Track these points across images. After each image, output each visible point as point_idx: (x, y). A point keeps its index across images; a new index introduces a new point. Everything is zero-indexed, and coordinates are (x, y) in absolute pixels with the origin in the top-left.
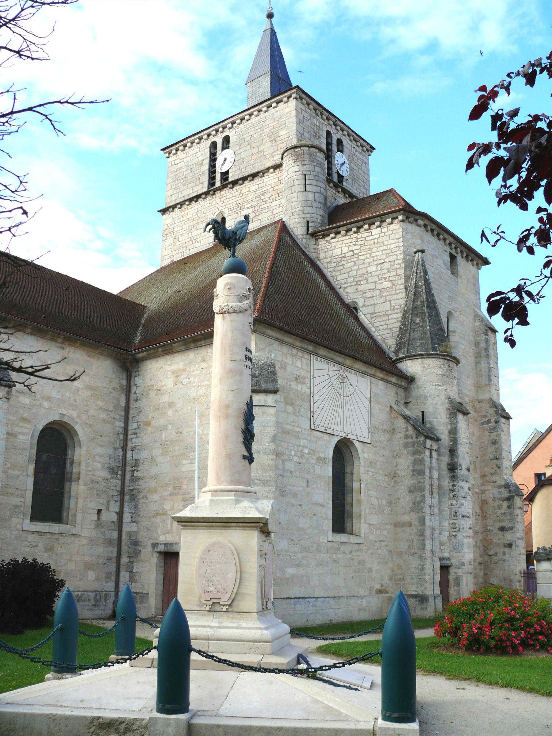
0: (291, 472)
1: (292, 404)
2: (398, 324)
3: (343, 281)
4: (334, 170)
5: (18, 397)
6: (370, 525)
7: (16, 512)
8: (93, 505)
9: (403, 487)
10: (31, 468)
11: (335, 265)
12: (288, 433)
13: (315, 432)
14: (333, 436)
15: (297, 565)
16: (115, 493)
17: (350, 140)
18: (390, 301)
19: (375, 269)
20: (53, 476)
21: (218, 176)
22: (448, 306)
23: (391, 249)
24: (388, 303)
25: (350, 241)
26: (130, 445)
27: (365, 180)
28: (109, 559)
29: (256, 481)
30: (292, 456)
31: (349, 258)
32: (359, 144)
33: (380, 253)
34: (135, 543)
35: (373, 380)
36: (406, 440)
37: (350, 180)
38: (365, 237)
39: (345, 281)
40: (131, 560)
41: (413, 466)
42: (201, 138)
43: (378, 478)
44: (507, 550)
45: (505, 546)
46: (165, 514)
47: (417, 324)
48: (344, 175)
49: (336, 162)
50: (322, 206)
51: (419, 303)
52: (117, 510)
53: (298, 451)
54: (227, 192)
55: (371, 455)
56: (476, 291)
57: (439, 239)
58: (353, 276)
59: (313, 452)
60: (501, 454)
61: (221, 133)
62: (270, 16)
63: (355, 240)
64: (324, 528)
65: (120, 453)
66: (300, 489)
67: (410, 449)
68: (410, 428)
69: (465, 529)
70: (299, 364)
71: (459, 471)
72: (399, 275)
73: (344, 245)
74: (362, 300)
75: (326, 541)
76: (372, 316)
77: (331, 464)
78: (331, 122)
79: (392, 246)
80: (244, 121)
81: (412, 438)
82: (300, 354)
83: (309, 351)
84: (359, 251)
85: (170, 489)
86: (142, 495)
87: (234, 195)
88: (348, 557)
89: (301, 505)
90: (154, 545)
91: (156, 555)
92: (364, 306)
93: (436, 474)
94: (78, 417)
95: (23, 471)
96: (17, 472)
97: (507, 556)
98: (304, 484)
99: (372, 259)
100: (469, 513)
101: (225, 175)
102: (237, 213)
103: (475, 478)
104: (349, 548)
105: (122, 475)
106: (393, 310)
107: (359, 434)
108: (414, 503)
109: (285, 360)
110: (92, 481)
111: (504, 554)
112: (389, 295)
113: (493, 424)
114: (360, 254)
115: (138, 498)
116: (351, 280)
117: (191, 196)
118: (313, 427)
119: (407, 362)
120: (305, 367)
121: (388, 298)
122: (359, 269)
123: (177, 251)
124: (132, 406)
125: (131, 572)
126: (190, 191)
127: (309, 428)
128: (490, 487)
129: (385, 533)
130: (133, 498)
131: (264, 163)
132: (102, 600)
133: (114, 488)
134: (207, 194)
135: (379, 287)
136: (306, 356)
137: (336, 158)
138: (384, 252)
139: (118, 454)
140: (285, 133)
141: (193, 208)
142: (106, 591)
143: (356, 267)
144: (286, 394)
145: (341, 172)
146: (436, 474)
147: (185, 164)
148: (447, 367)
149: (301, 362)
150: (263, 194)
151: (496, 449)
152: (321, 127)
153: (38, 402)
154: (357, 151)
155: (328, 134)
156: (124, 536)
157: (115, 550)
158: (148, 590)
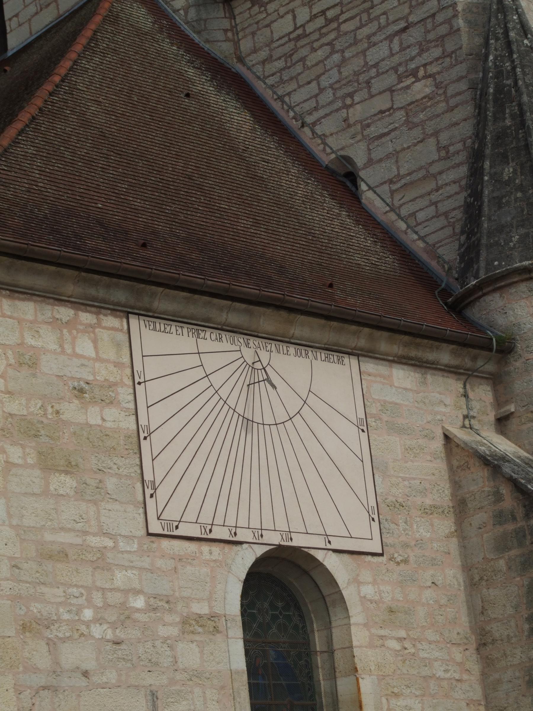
1: (70, 468)
3: (307, 106)
11: (280, 64)
12: (61, 555)
13: (165, 543)
14: (235, 548)
18: (436, 134)
19: (387, 52)
24: (432, 141)
31: (316, 36)
35: (369, 366)
36: (499, 530)
39: (312, 103)
43: (422, 654)
47: (507, 183)
51: (508, 122)
53: (107, 606)
55: (389, 588)
67: (514, 552)
68: (505, 490)
70: (85, 347)
72: (450, 56)
74: (363, 146)
76: (394, 187)
77: (236, 633)
81: (514, 518)
82: (86, 317)
83: (118, 304)
92: (370, 162)
106: (447, 158)
109: (30, 341)
112: (430, 119)
116: (328, 96)
118: (155, 527)
119: (488, 298)
120: (110, 354)
122: (344, 60)
127: (143, 532)
135: (401, 100)
143: (336, 57)
144: (43, 439)
149: (95, 342)
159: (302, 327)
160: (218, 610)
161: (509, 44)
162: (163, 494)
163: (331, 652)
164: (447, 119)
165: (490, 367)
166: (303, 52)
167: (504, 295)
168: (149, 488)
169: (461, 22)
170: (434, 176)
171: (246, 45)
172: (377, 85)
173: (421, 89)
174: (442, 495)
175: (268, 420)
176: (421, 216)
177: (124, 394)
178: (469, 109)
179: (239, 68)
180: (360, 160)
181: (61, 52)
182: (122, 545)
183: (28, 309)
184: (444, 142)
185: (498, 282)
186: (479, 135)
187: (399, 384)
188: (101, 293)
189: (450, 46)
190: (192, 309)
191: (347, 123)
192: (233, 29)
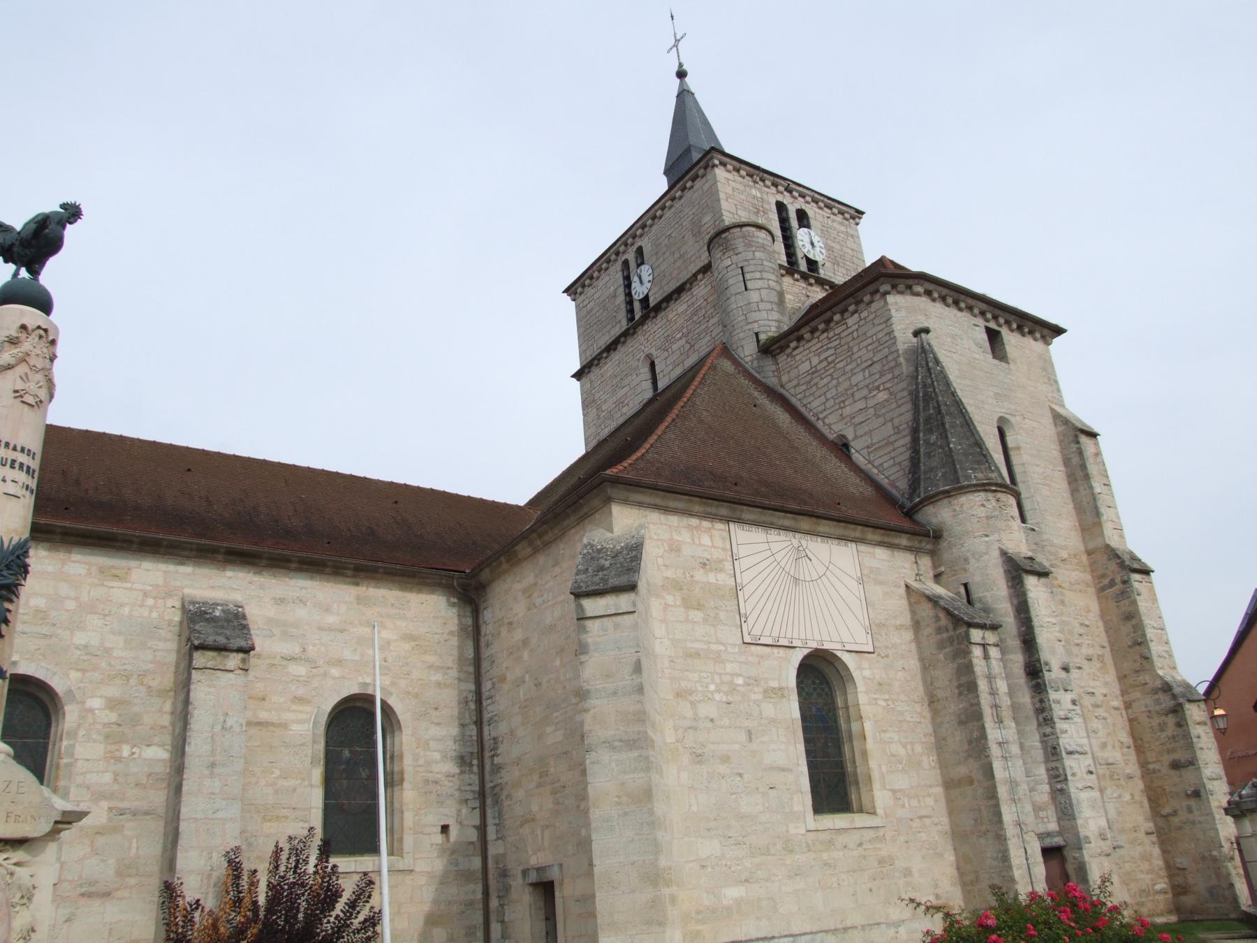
0: (712, 720)
1: (699, 607)
2: (907, 455)
3: (820, 409)
4: (800, 255)
5: (285, 667)
6: (894, 791)
8: (433, 819)
10: (317, 773)
11: (804, 387)
12: (697, 655)
13: (753, 647)
15: (746, 881)
16: (470, 796)
17: (820, 208)
21: (637, 306)
22: (998, 410)
23: (878, 340)
24: (889, 425)
25: (819, 345)
26: (486, 716)
27: (855, 260)
28: (471, 904)
29: (617, 744)
30: (712, 693)
32: (835, 211)
33: (864, 351)
34: (504, 874)
35: (862, 548)
36: (939, 637)
37: (828, 264)
39: (822, 407)
41: (958, 679)
44: (1192, 802)
45: (1188, 796)
46: (533, 820)
48: (817, 259)
49: (800, 243)
50: (775, 307)
52: (477, 822)
56: (1049, 379)
57: (960, 310)
59: (753, 681)
60: (1144, 635)
62: (681, 74)
63: (826, 341)
64: (795, 809)
65: (473, 731)
66: (736, 747)
68: (942, 615)
69: (1079, 774)
70: (706, 540)
71: (1046, 674)
75: (803, 831)
78: (781, 188)
79: (880, 336)
82: (706, 524)
85: (536, 777)
86: (505, 793)
88: (856, 853)
89: (740, 775)
91: (528, 890)
92: (856, 437)
93: (1002, 686)
94: (393, 684)
95: (303, 779)
96: (291, 783)
97: (1196, 813)
98: (743, 737)
99: (854, 364)
100: (1081, 746)
101: (645, 300)
103: (1106, 684)
104: (856, 837)
107: (846, 637)
108: (970, 742)
109: (676, 537)
110: (427, 781)
111: (1190, 810)
113: (1119, 586)
116: (831, 403)
118: (747, 639)
120: (719, 543)
121: (888, 417)
124: (483, 656)
125: (503, 922)
128: (1138, 695)
129: (930, 801)
130: (497, 802)
133: (468, 788)
134: (626, 334)
135: (871, 403)
136: (719, 526)
137: (799, 237)
143: (835, 382)
145: (811, 256)
146: (1002, 686)
148: (993, 502)
149: (711, 537)
151: (1134, 627)
152: (765, 197)
153: (321, 671)
154: (833, 221)
155: (781, 207)
159: (825, 526)
160: (784, 685)
161: (929, 369)
162: (751, 621)
163: (847, 708)
164: (898, 411)
165: (929, 547)
166: (816, 380)
167: (62, 783)
168: (742, 617)
169: (902, 359)
170: (892, 443)
171: (785, 378)
172: (858, 396)
173: (882, 396)
174: (906, 619)
175: (808, 579)
176: (886, 465)
177: (728, 566)
178: (909, 406)
179: (782, 391)
180: (850, 436)
181: (686, 387)
182: (729, 649)
183: (674, 520)
184: (896, 424)
185: (931, 499)
186: (916, 419)
187: (879, 558)
188: (714, 510)
189: (897, 373)
190: (763, 518)
191: (842, 417)
192: (778, 370)
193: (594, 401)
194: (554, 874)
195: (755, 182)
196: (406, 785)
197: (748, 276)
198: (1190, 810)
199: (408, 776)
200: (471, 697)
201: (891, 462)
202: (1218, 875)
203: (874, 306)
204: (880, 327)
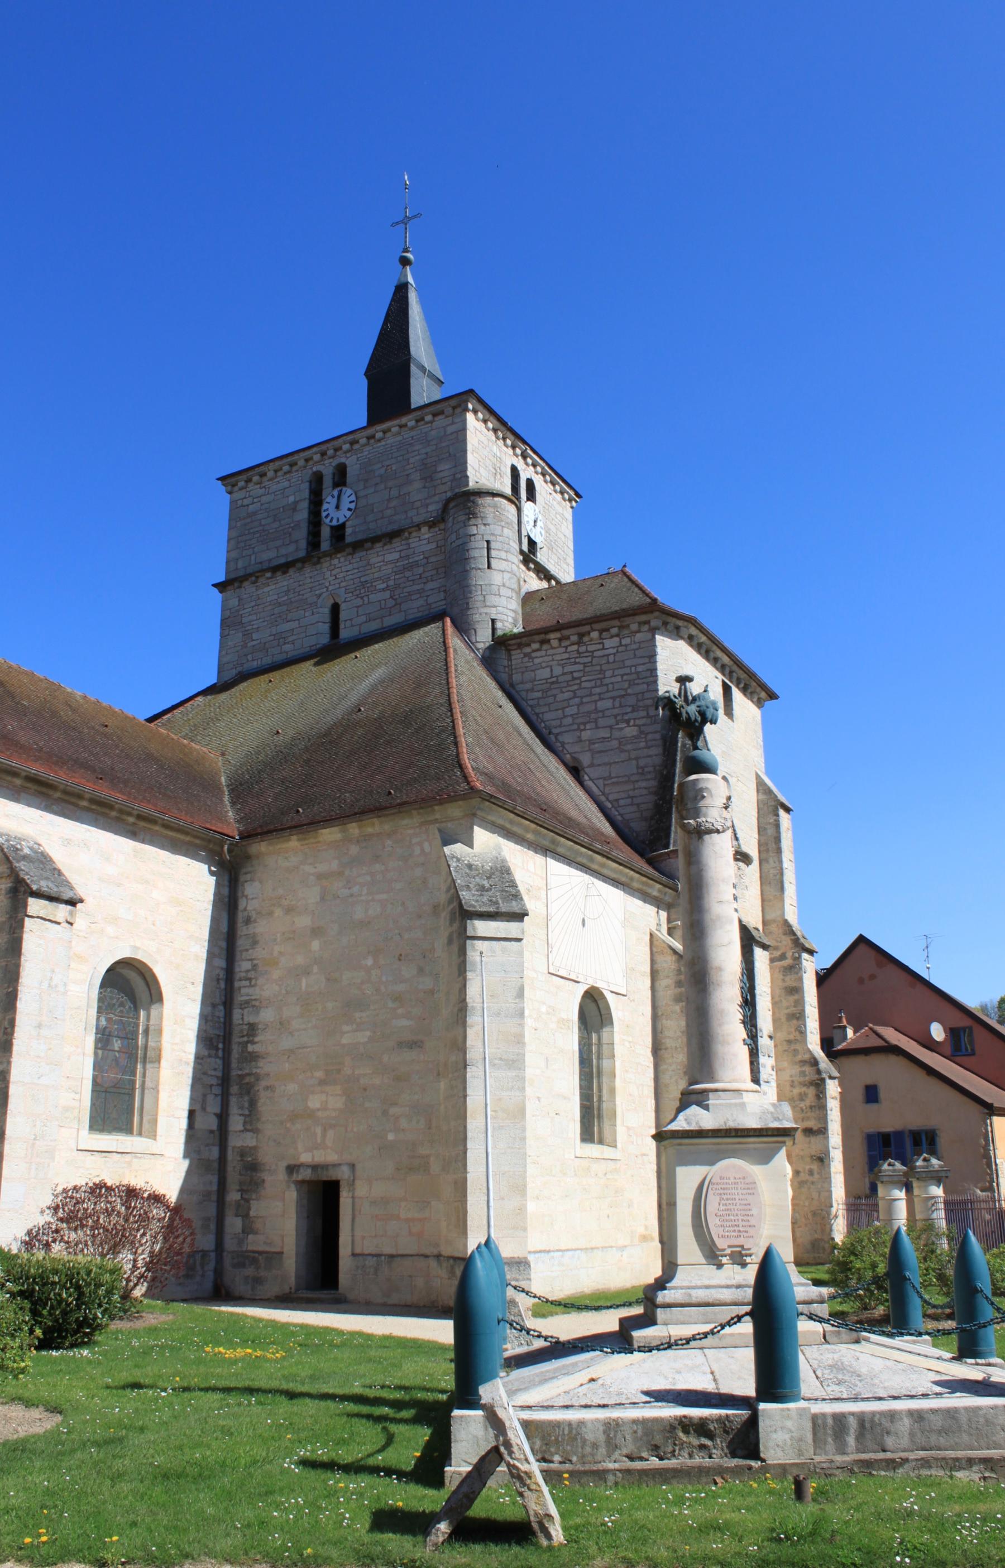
3: (554, 723)
6: (628, 1128)
7: (67, 1118)
9: (674, 1067)
11: (539, 694)
16: (214, 1081)
17: (546, 482)
20: (117, 1054)
21: (325, 532)
23: (637, 673)
25: (566, 656)
33: (619, 679)
34: (252, 1167)
36: (679, 990)
38: (593, 652)
39: (558, 722)
40: (245, 1196)
42: (292, 465)
50: (514, 595)
54: (342, 559)
58: (571, 715)
61: (330, 458)
65: (220, 1012)
73: (555, 663)
79: (640, 669)
80: (372, 441)
84: (580, 674)
86: (263, 1083)
87: (355, 565)
89: (539, 1099)
90: (291, 1169)
91: (293, 1186)
92: (592, 765)
95: (77, 1047)
99: (605, 688)
101: (338, 531)
102: (362, 598)
105: (224, 1050)
113: (789, 961)
114: (583, 679)
115: (256, 1088)
116: (568, 721)
117: (275, 563)
123: (250, 657)
126: (271, 554)
130: (248, 1090)
131: (410, 514)
132: (198, 1267)
133: (213, 1073)
135: (617, 734)
138: (625, 677)
139: (217, 1014)
140: (447, 467)
141: (280, 584)
142: (202, 1251)
143: (577, 700)
147: (263, 507)
150: (410, 567)
155: (514, 470)
156: (230, 1155)
157: (215, 1179)
158: (282, 1247)
193: (241, 623)
194: (343, 1174)
195: (497, 438)
196: (164, 1063)
197: (493, 553)
198: (811, 1173)
199: (166, 1054)
200: (222, 974)
201: (629, 801)
202: (823, 1231)
203: (639, 637)
204: (642, 661)
